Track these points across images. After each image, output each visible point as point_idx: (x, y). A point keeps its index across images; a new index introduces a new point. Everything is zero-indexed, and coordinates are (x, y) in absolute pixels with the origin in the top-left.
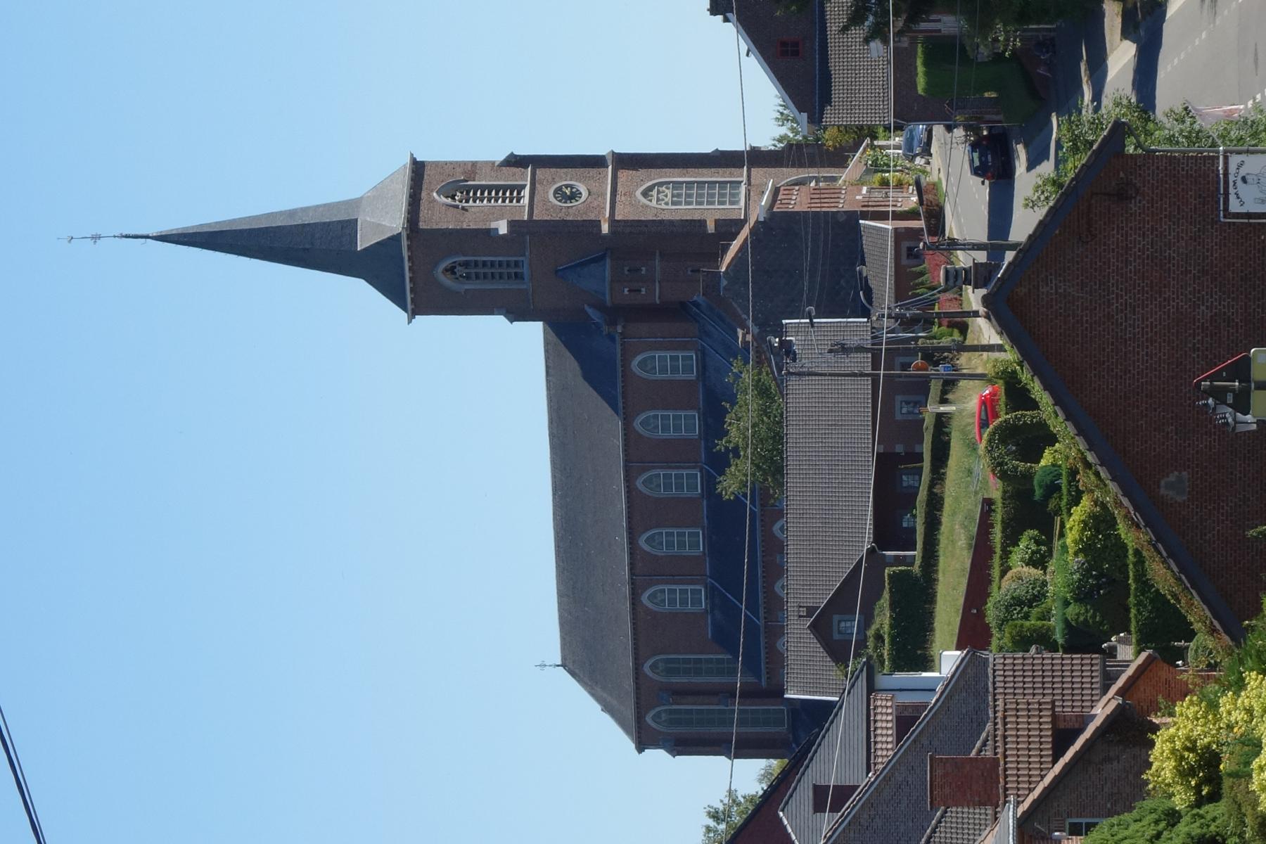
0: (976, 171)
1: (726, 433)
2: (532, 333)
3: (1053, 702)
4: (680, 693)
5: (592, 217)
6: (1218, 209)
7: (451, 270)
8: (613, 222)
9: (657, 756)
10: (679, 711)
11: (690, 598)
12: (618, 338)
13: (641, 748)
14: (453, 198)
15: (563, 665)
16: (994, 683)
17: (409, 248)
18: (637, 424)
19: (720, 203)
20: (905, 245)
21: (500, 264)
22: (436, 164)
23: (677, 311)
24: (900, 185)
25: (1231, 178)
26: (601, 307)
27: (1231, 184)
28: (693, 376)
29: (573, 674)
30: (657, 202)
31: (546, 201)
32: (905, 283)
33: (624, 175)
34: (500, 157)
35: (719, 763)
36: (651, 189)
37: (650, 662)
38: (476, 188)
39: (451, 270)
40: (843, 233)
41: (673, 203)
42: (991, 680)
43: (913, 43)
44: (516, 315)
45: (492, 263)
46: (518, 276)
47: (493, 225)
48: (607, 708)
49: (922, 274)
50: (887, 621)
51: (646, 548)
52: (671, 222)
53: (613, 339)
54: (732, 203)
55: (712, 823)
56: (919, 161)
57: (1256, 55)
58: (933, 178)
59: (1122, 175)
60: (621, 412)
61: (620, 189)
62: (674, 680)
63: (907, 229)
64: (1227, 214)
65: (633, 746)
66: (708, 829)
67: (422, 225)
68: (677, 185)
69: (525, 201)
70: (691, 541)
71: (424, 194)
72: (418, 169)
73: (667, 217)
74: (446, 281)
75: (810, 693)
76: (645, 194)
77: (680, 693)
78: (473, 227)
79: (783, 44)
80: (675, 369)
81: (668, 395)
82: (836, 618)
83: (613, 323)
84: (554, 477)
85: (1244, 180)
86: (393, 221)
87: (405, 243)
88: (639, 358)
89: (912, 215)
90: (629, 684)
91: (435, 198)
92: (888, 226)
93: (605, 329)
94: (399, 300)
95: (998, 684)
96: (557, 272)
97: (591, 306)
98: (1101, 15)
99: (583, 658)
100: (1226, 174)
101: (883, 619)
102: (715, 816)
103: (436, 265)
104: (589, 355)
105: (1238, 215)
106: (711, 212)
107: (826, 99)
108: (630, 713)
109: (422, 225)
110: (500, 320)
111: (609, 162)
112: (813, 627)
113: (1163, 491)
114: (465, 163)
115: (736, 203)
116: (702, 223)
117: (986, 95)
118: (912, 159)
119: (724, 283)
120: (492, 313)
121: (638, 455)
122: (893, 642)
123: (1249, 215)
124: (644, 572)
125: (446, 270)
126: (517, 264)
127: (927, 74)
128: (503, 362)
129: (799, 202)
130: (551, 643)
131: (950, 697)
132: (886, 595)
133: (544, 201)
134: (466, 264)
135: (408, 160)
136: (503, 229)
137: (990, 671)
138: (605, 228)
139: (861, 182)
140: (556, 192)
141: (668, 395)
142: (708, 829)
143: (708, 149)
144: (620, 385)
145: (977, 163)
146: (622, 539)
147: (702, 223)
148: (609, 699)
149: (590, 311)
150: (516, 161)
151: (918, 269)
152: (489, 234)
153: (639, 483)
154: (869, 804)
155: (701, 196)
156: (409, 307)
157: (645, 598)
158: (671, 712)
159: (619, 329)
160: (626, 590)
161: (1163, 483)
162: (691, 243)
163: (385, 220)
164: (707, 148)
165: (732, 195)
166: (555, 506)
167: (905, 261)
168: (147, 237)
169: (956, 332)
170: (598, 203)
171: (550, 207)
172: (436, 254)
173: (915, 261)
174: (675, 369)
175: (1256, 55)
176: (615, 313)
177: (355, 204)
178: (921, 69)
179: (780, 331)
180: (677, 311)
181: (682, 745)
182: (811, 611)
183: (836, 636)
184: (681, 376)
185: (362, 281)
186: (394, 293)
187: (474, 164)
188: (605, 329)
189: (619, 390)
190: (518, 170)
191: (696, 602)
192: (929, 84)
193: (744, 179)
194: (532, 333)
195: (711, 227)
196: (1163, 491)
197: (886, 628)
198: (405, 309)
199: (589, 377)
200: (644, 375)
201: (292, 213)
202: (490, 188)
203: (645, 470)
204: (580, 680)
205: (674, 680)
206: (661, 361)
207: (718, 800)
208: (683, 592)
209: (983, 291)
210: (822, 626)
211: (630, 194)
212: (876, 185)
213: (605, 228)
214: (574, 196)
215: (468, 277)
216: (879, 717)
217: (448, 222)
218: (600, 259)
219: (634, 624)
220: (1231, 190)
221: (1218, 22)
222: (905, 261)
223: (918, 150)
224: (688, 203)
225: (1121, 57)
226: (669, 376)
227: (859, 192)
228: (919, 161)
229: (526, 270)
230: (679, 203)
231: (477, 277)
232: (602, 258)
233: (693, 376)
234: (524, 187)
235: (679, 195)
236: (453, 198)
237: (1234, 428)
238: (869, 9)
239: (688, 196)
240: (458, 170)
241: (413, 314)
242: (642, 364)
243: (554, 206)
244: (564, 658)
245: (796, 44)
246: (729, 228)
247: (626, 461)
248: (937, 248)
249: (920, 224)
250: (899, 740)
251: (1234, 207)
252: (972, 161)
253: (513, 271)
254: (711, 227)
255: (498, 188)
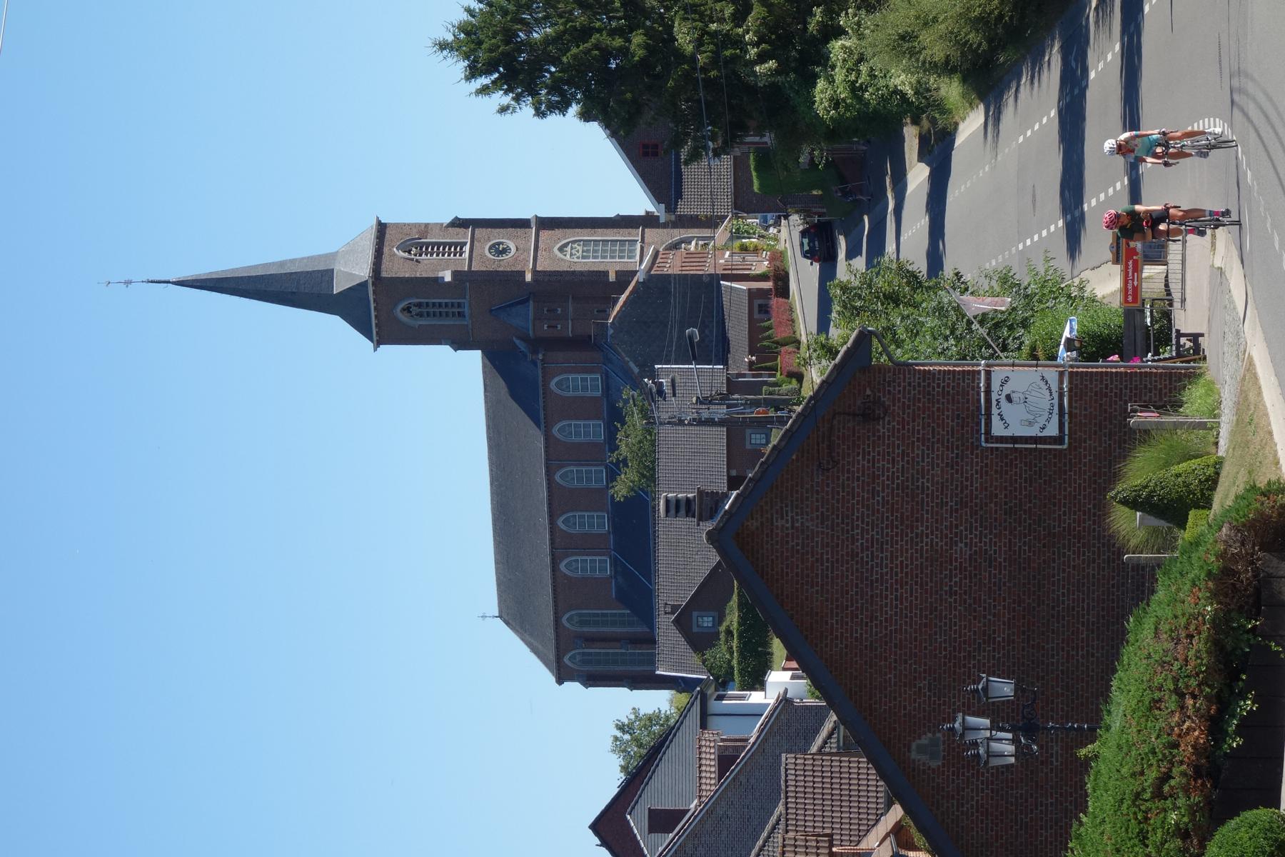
0: (806, 255)
1: (617, 448)
2: (474, 358)
3: (831, 835)
4: (590, 640)
5: (518, 268)
6: (978, 431)
7: (407, 309)
8: (535, 272)
9: (573, 688)
10: (590, 654)
11: (598, 566)
12: (539, 364)
13: (560, 681)
14: (409, 252)
15: (500, 617)
16: (786, 781)
17: (374, 292)
18: (555, 430)
19: (620, 257)
20: (757, 302)
21: (446, 305)
22: (397, 225)
23: (581, 343)
24: (756, 250)
25: (994, 397)
26: (525, 339)
27: (994, 403)
28: (599, 394)
29: (507, 623)
30: (570, 256)
31: (482, 256)
32: (755, 332)
33: (545, 235)
34: (447, 220)
35: (622, 692)
36: (566, 245)
37: (567, 616)
38: (427, 245)
39: (407, 309)
40: (703, 293)
41: (583, 257)
42: (783, 778)
43: (746, 155)
44: (460, 343)
45: (440, 305)
46: (461, 315)
47: (440, 274)
48: (534, 650)
49: (769, 328)
50: (736, 619)
51: (563, 527)
52: (581, 273)
53: (536, 365)
54: (629, 257)
55: (619, 734)
56: (772, 230)
57: (1034, 196)
58: (781, 247)
59: (868, 392)
60: (543, 426)
61: (541, 245)
62: (585, 629)
63: (759, 290)
64: (989, 437)
65: (554, 679)
66: (616, 739)
67: (384, 274)
68: (586, 242)
69: (466, 255)
70: (598, 523)
71: (386, 250)
72: (382, 228)
73: (578, 268)
74: (404, 318)
75: (677, 671)
76: (561, 249)
77: (590, 640)
78: (425, 275)
79: (645, 146)
80: (585, 388)
81: (579, 408)
82: (695, 614)
83: (535, 352)
84: (491, 470)
85: (1009, 398)
86: (362, 271)
87: (371, 289)
88: (556, 380)
89: (762, 277)
90: (550, 633)
91: (395, 253)
92: (742, 286)
93: (530, 357)
94: (367, 333)
95: (790, 777)
96: (491, 311)
97: (518, 338)
98: (901, 140)
99: (515, 611)
100: (988, 391)
101: (733, 618)
102: (621, 728)
103: (396, 305)
104: (517, 384)
105: (1002, 439)
106: (611, 265)
107: (679, 195)
108: (552, 656)
109: (384, 274)
110: (446, 349)
111: (533, 225)
112: (676, 622)
113: (914, 755)
114: (420, 225)
115: (634, 257)
116: (606, 273)
117: (815, 192)
118: (767, 229)
119: (611, 332)
120: (440, 343)
121: (556, 456)
122: (740, 636)
123: (1014, 439)
124: (561, 546)
125: (403, 310)
126: (459, 305)
127: (758, 177)
128: (452, 380)
129: (673, 265)
130: (491, 602)
131: (765, 740)
132: (735, 597)
133: (480, 256)
134: (419, 305)
135: (374, 222)
136: (448, 278)
137: (783, 770)
138: (528, 277)
139: (725, 247)
140: (490, 248)
141: (579, 408)
142: (616, 739)
143: (611, 214)
144: (541, 400)
145: (806, 248)
146: (544, 520)
147: (606, 273)
148: (535, 643)
149: (517, 342)
150: (459, 223)
151: (766, 324)
152: (437, 281)
153: (557, 477)
154: (694, 835)
155: (605, 251)
156: (375, 338)
157: (562, 566)
158: (584, 654)
159: (540, 356)
160: (548, 559)
161: (914, 746)
162: (594, 289)
163: (355, 269)
164: (610, 213)
165: (630, 251)
166: (492, 494)
167: (756, 316)
168: (168, 282)
169: (794, 381)
170: (522, 257)
171: (485, 260)
172: (397, 301)
173: (763, 316)
174: (585, 388)
175: (1034, 196)
176: (538, 344)
177: (333, 256)
178: (754, 174)
179: (653, 375)
180: (581, 343)
181: (592, 680)
182: (675, 608)
183: (695, 629)
184: (589, 394)
185: (577, 684)
186: (362, 326)
187: (427, 225)
188: (530, 357)
189: (541, 404)
190: (462, 230)
191: (603, 569)
192: (761, 186)
193: (640, 238)
194: (474, 358)
195: (612, 277)
196: (914, 755)
197: (735, 625)
198: (371, 340)
199: (513, 395)
200: (559, 392)
201: (282, 264)
202: (439, 244)
203: (562, 467)
204: (513, 629)
205: (585, 629)
206: (574, 382)
207: (625, 716)
208: (587, 434)
209: (709, 526)
210: (683, 621)
211: (550, 250)
212: (737, 250)
213: (528, 277)
214: (505, 251)
215: (420, 315)
216: (703, 762)
217: (405, 272)
218: (524, 302)
219: (555, 591)
220: (995, 411)
221: (999, 158)
222: (756, 316)
223: (771, 222)
224: (595, 257)
225: (918, 175)
226: (580, 393)
227: (723, 257)
228: (772, 230)
229: (466, 310)
230: (588, 257)
231: (428, 314)
232: (527, 300)
233: (599, 394)
234: (465, 244)
235: (588, 251)
236: (409, 252)
237: (987, 763)
238: (688, 134)
239: (595, 251)
240: (415, 230)
241: (379, 343)
242: (558, 384)
243: (489, 259)
244: (500, 611)
245: (656, 146)
246: (625, 277)
247: (547, 460)
248: (710, 403)
249: (768, 285)
250: (720, 776)
251: (998, 429)
252: (802, 245)
253: (456, 310)
254: (612, 277)
255: (445, 244)
